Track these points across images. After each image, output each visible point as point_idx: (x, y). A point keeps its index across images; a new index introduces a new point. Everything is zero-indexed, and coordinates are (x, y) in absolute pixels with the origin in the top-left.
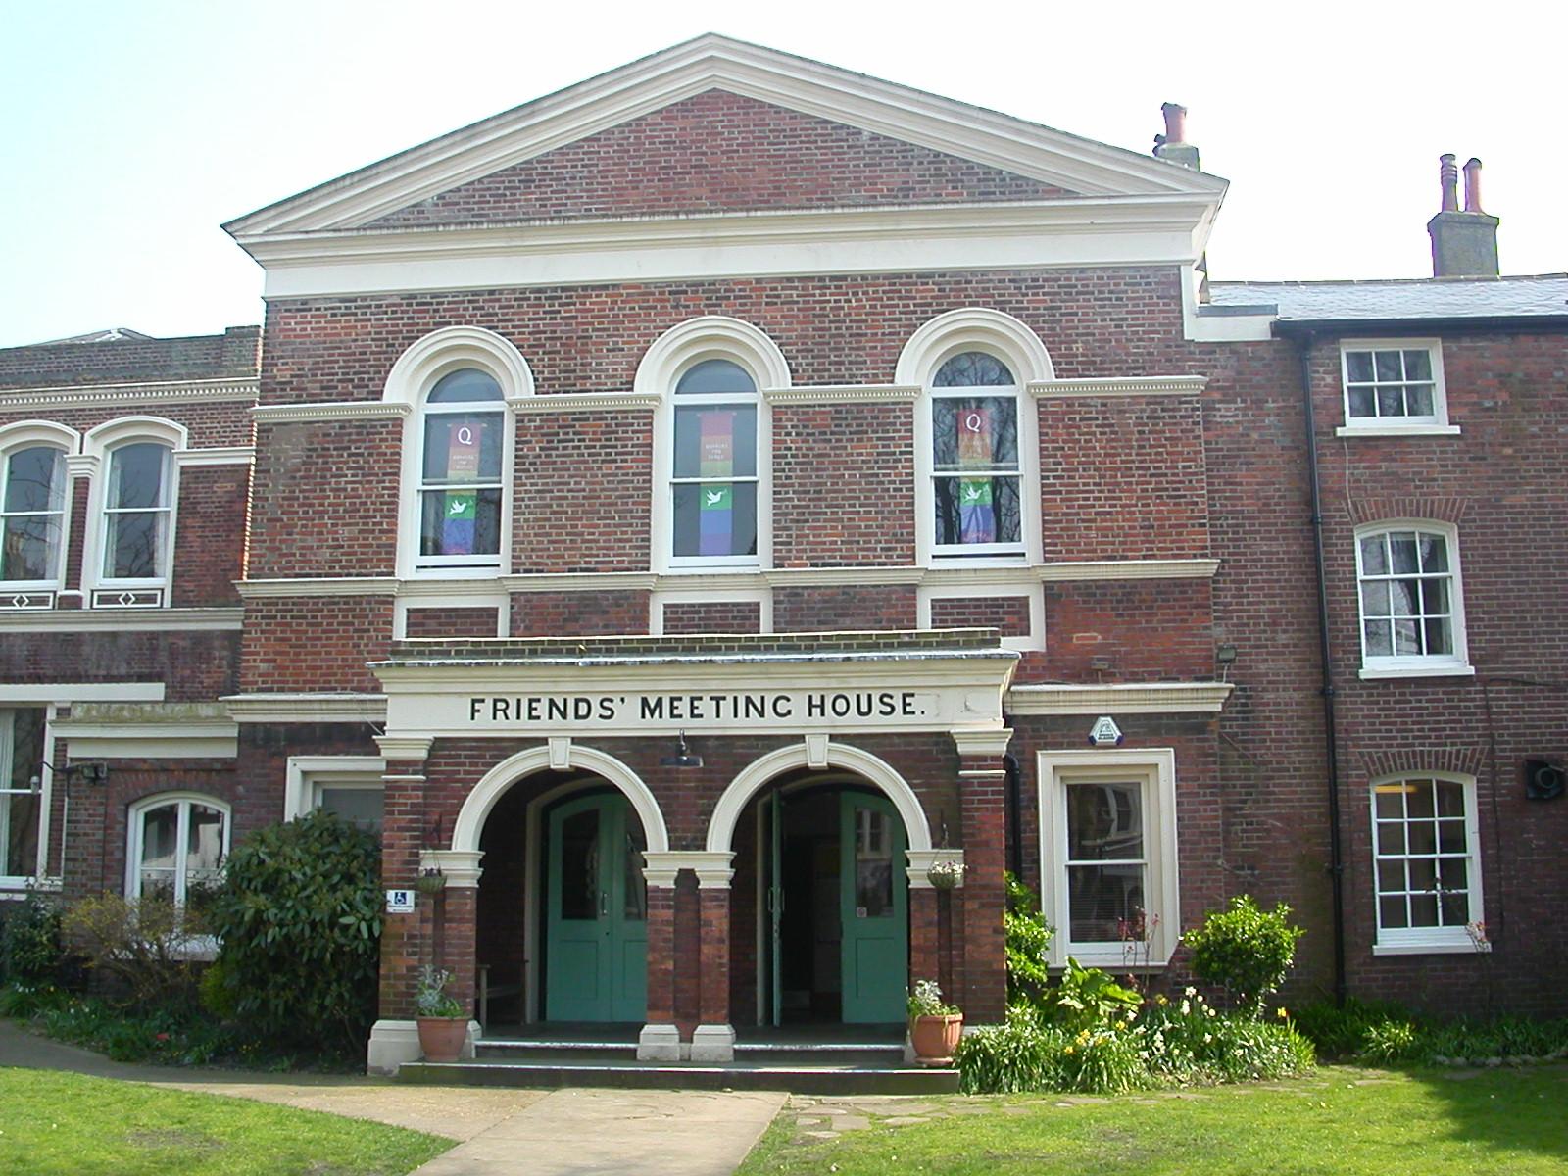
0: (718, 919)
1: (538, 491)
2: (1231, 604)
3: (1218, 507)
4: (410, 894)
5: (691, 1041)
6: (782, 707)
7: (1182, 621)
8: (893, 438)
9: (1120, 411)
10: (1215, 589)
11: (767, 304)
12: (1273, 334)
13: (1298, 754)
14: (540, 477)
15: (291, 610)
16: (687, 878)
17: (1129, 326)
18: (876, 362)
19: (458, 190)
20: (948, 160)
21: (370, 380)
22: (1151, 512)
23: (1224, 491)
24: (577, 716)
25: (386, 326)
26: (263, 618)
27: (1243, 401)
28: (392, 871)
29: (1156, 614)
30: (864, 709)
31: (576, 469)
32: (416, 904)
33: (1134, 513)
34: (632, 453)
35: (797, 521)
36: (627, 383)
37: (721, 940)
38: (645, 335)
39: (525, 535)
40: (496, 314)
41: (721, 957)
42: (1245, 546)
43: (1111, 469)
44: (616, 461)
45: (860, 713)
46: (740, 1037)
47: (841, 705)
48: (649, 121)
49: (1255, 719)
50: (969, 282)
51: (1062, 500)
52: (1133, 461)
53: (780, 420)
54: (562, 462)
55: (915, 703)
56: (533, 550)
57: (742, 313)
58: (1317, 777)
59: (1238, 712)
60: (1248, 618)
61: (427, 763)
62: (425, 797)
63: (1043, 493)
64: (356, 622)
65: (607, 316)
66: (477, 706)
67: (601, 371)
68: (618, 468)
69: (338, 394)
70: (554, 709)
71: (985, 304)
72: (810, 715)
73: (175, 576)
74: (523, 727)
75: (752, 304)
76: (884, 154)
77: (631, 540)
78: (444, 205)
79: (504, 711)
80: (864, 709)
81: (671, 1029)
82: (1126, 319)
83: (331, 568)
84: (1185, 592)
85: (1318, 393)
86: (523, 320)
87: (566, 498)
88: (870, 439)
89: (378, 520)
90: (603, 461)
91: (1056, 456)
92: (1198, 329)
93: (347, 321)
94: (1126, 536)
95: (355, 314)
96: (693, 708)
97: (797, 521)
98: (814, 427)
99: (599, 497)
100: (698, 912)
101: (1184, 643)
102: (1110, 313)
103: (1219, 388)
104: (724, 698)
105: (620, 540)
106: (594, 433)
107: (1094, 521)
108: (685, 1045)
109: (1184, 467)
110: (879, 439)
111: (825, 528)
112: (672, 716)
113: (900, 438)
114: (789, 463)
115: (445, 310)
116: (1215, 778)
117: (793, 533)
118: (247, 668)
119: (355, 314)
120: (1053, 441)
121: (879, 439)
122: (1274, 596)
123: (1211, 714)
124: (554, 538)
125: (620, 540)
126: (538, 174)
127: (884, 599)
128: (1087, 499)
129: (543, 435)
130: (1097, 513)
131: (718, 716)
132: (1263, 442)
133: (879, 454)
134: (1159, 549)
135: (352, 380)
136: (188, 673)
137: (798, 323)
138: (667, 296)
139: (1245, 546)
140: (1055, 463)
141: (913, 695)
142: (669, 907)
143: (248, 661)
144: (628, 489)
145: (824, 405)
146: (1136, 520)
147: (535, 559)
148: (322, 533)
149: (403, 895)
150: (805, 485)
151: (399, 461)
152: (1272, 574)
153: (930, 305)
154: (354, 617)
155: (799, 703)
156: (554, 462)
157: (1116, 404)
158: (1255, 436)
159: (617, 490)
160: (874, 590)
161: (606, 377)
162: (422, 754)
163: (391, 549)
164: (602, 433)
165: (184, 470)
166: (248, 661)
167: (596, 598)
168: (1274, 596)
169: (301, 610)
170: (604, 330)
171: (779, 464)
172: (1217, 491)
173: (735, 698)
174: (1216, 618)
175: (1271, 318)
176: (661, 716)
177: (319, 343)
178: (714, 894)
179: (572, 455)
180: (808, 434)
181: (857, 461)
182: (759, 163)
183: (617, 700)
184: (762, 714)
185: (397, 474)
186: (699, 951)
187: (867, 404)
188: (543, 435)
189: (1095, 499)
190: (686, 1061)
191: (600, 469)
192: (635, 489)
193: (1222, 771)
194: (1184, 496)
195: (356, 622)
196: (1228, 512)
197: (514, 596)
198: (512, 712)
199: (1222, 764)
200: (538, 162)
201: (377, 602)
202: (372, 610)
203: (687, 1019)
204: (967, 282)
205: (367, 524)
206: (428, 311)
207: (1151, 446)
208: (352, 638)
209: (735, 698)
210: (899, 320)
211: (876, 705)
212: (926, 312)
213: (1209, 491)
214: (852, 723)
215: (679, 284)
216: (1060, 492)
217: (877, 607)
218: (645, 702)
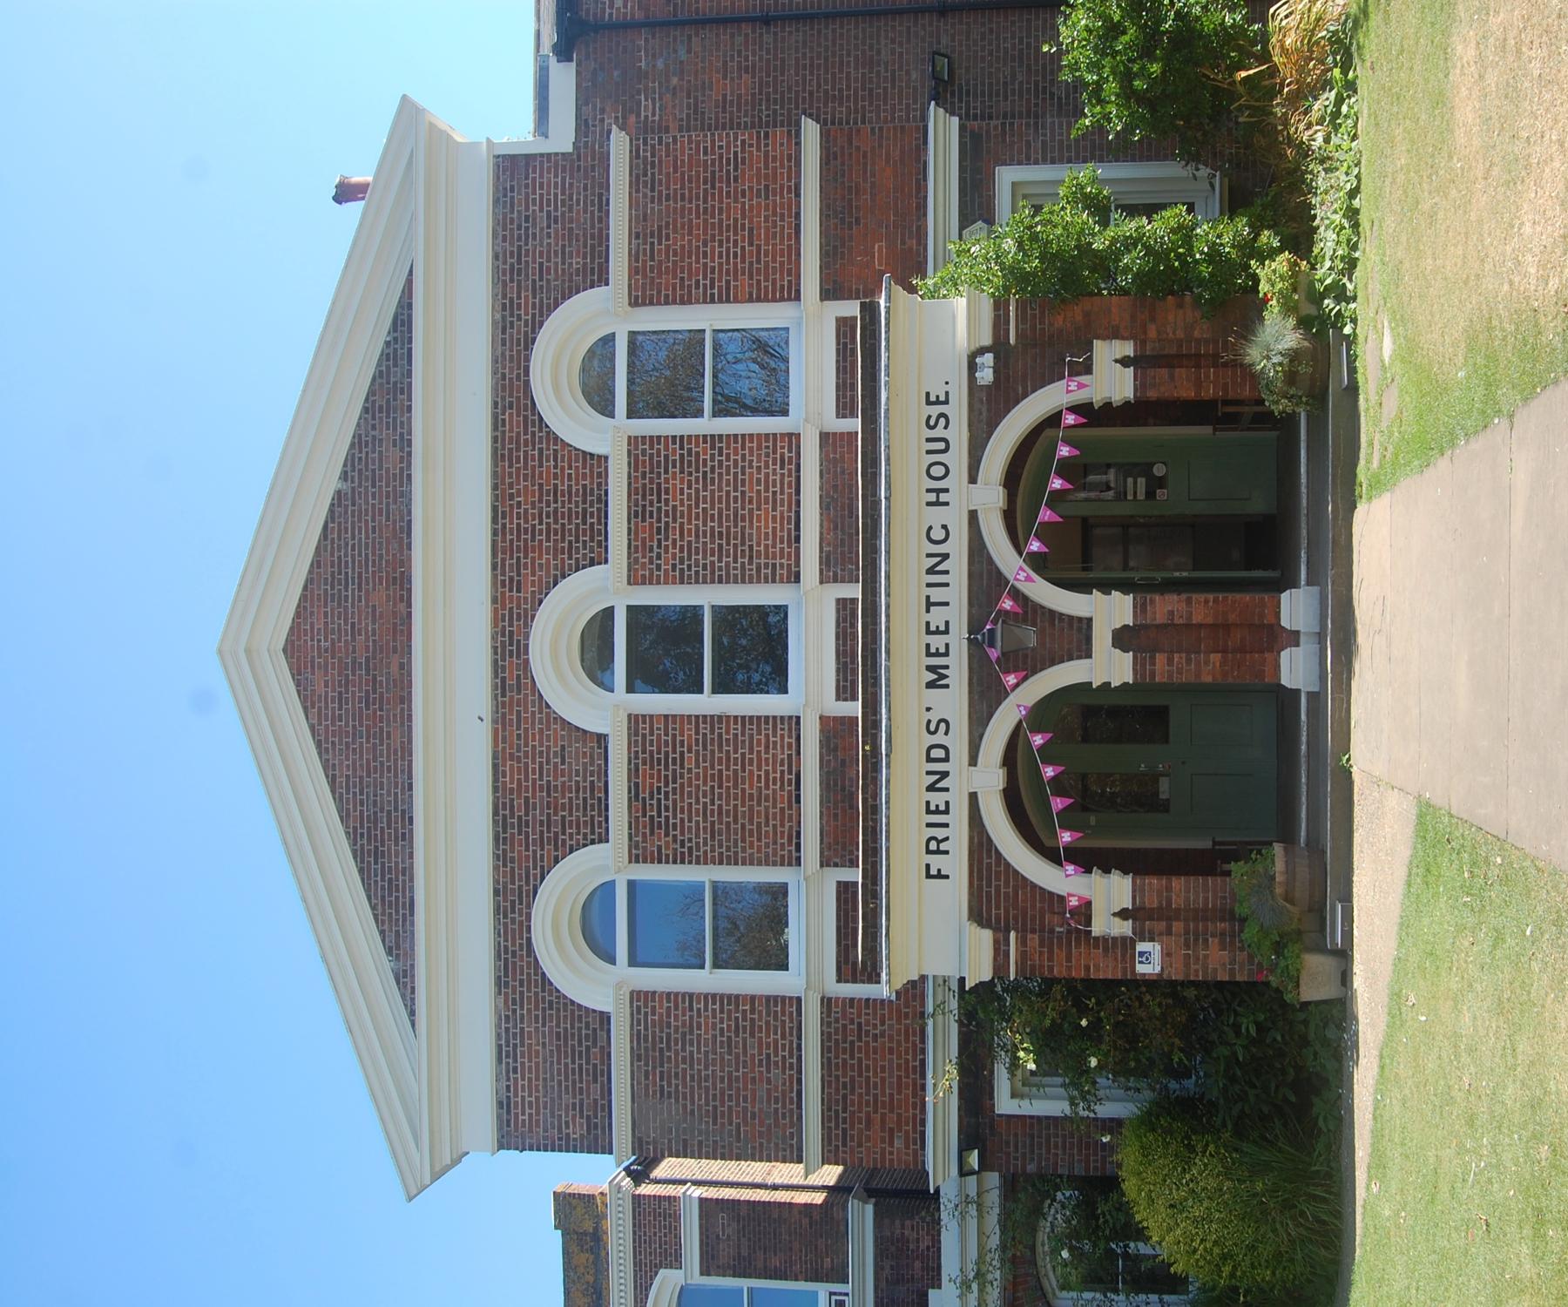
0: (1166, 606)
1: (713, 837)
2: (848, 108)
3: (748, 120)
4: (1141, 947)
5: (1298, 632)
6: (938, 534)
7: (865, 156)
8: (666, 457)
9: (645, 220)
10: (833, 123)
11: (519, 591)
12: (570, 60)
13: (1005, 39)
14: (697, 836)
15: (837, 1112)
16: (1122, 638)
17: (556, 209)
18: (584, 475)
19: (382, 933)
20: (371, 399)
21: (587, 1027)
22: (751, 188)
23: (731, 113)
24: (946, 759)
25: (529, 1010)
26: (844, 1145)
27: (639, 93)
28: (1115, 967)
29: (857, 184)
30: (942, 445)
31: (690, 796)
32: (1152, 940)
33: (751, 206)
34: (674, 736)
35: (751, 557)
36: (599, 742)
37: (1189, 601)
38: (548, 721)
39: (759, 851)
40: (520, 887)
41: (1207, 602)
42: (790, 91)
43: (705, 229)
44: (682, 754)
45: (946, 450)
46: (1294, 584)
47: (938, 471)
48: (315, 721)
49: (968, 84)
50: (504, 376)
51: (736, 279)
52: (698, 206)
53: (643, 576)
54: (682, 812)
55: (938, 391)
56: (775, 843)
57: (528, 618)
58: (1029, 21)
59: (960, 101)
60: (864, 89)
61: (996, 930)
62: (1033, 931)
63: (728, 301)
64: (850, 1038)
65: (526, 764)
66: (933, 872)
67: (585, 770)
68: (690, 751)
69: (602, 1063)
70: (938, 786)
71: (527, 359)
72: (947, 504)
73: (817, 1280)
74: (959, 821)
75: (519, 607)
76: (363, 466)
77: (767, 736)
78: (398, 948)
79: (939, 842)
80: (942, 445)
81: (1285, 655)
82: (549, 212)
83: (791, 1068)
84: (835, 154)
85: (633, 15)
86: (527, 857)
87: (720, 807)
88: (667, 481)
89: (739, 1015)
90: (682, 767)
91: (690, 286)
92: (562, 139)
93: (523, 1056)
94: (775, 214)
95: (515, 1045)
96: (937, 632)
97: (751, 557)
98: (652, 540)
99: (720, 771)
100: (1157, 626)
101: (888, 154)
102: (542, 229)
103: (624, 117)
104: (928, 597)
105: (767, 747)
106: (652, 777)
107: (759, 247)
108: (1302, 639)
109: (705, 153)
110: (666, 472)
111: (759, 528)
112: (946, 654)
113: (667, 449)
114: (689, 567)
115: (514, 944)
116: (1028, 125)
117: (763, 561)
118: (899, 1160)
119: (515, 1045)
120: (674, 289)
121: (666, 472)
122: (841, 63)
123: (962, 128)
124: (763, 820)
125: (767, 747)
126: (369, 843)
127: (835, 467)
128: (735, 254)
129: (652, 833)
130: (751, 244)
131: (947, 604)
132: (682, 72)
133: (682, 472)
134: (789, 180)
135: (588, 1048)
136: (918, 1264)
137: (540, 557)
138: (506, 699)
139: (790, 91)
140: (697, 287)
141: (928, 394)
142: (1153, 658)
143: (891, 1161)
144: (712, 739)
145: (629, 529)
146: (759, 204)
147: (785, 840)
148: (754, 1078)
149: (1141, 954)
150: (712, 550)
151: (677, 994)
152: (819, 65)
153: (526, 417)
154: (845, 1042)
155: (936, 516)
156: (682, 820)
157: (637, 222)
158: (675, 80)
159: (713, 752)
160: (825, 476)
161: (592, 765)
162: (987, 935)
163: (771, 1000)
164: (652, 768)
165: (705, 1271)
166: (891, 1161)
167: (828, 772)
168: (841, 63)
169: (837, 1101)
170: (541, 768)
171: (690, 577)
172: (731, 120)
173: (929, 585)
174: (863, 122)
175: (553, 60)
176: (947, 667)
177: (545, 1087)
178: (1139, 609)
179: (675, 801)
180: (659, 546)
181: (689, 495)
182: (367, 600)
183: (929, 715)
184: (945, 556)
185: (691, 996)
186: (1200, 626)
187: (629, 484)
188: (652, 833)
189: (735, 245)
190: (1321, 637)
191: (690, 770)
192: (712, 732)
193: (1021, 117)
194: (736, 153)
195: (850, 1038)
196: (753, 110)
197: (825, 862)
198: (940, 833)
199: (1013, 117)
200: (355, 844)
201: (829, 1016)
202: (837, 1021)
203: (1276, 638)
204: (504, 378)
205: (744, 1027)
206: (514, 963)
207: (682, 188)
208: (867, 1043)
209: (929, 585)
210: (541, 450)
211: (939, 432)
212: (533, 422)
213: (732, 129)
214: (958, 458)
215: (495, 687)
216: (728, 282)
217: (843, 472)
218: (930, 685)
